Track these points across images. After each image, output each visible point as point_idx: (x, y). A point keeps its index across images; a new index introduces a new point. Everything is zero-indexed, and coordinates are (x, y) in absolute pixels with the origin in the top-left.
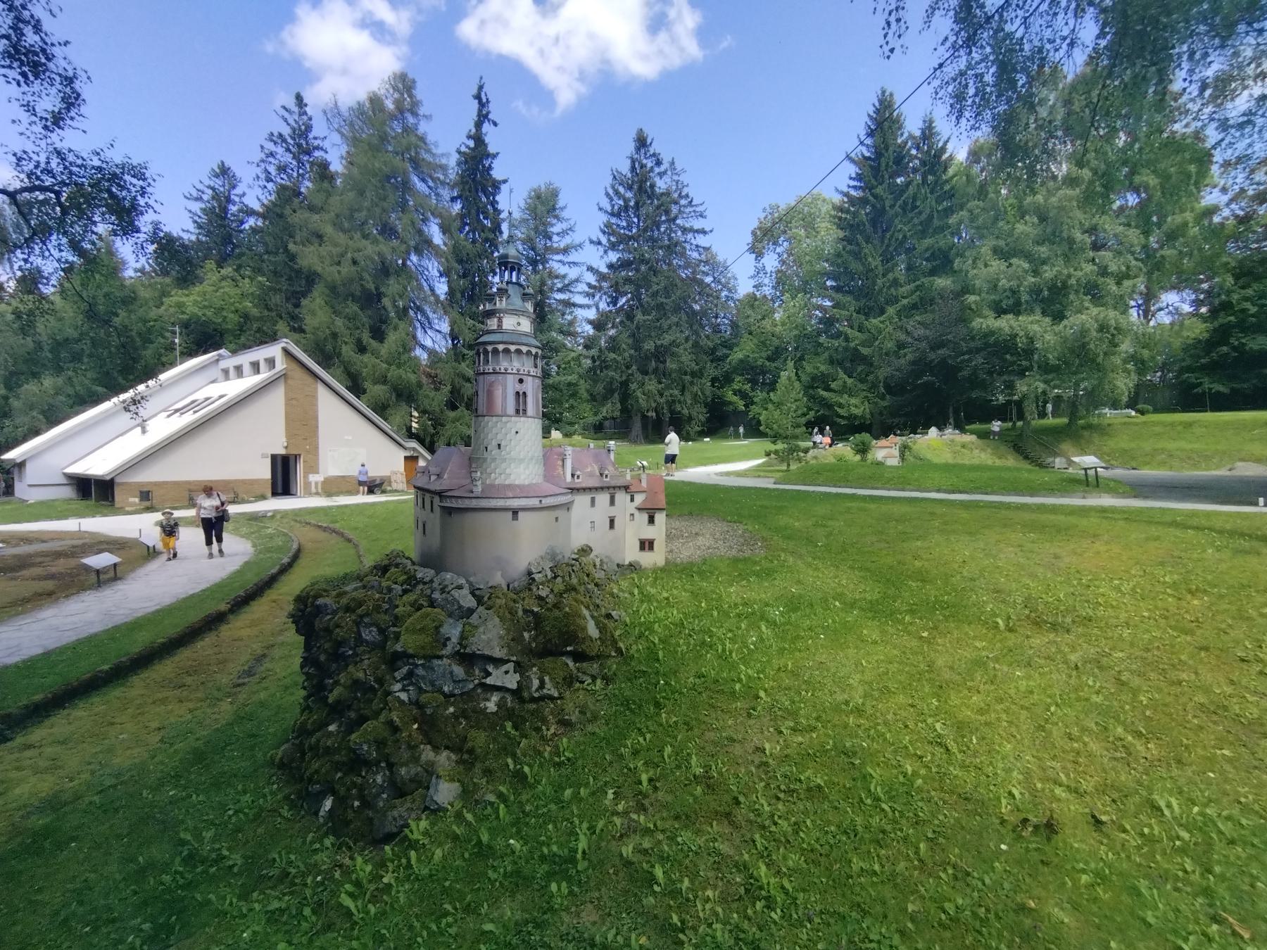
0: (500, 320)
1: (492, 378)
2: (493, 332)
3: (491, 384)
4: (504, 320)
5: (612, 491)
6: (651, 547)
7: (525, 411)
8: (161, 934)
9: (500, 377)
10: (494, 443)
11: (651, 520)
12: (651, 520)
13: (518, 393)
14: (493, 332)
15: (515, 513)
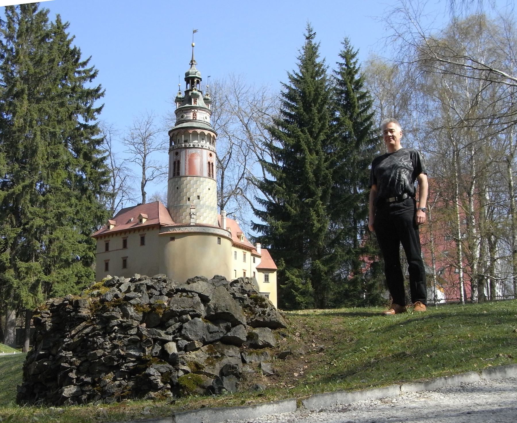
0: (195, 115)
1: (193, 151)
2: (190, 121)
3: (192, 155)
4: (198, 114)
9: (199, 151)
10: (195, 195)
11: (267, 279)
12: (267, 279)
13: (209, 163)
14: (190, 121)
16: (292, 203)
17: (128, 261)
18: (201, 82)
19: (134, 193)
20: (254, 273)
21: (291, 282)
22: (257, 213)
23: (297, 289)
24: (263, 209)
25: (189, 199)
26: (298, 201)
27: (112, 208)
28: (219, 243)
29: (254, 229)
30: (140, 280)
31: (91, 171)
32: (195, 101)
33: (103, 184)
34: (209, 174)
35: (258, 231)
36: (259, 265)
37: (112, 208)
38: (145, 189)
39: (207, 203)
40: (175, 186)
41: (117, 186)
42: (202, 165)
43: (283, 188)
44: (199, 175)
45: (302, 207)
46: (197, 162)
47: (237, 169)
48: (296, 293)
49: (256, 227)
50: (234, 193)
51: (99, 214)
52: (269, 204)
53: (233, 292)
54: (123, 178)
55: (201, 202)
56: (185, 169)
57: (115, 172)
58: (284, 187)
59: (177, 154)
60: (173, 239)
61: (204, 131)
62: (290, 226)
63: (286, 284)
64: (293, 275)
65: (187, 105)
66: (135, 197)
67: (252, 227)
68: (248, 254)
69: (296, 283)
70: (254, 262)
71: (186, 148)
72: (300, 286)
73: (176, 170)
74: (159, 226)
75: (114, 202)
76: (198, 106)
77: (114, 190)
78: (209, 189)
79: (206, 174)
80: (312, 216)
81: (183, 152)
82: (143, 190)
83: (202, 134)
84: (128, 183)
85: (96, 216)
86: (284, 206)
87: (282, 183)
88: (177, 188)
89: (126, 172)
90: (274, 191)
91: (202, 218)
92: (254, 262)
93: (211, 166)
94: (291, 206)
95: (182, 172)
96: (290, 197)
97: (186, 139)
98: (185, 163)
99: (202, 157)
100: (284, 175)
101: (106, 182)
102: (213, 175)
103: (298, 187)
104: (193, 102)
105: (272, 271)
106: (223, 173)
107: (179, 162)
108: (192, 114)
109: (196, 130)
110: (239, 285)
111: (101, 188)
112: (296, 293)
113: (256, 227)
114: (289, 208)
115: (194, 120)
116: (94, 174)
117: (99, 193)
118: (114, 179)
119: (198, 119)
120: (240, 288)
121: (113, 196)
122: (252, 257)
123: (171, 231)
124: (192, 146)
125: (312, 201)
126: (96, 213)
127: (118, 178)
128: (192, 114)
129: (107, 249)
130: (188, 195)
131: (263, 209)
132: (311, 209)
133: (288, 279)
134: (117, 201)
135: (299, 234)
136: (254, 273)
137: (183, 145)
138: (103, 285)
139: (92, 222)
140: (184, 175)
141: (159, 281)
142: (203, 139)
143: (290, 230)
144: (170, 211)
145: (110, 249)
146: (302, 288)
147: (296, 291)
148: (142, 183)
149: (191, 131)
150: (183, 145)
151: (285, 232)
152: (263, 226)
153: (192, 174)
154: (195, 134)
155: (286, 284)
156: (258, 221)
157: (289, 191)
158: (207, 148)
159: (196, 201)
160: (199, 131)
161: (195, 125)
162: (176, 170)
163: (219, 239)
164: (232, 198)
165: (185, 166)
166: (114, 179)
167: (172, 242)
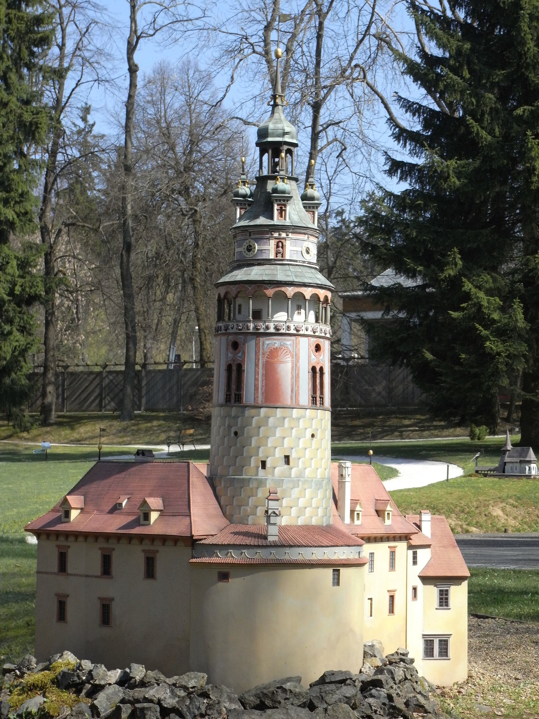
0: (280, 245)
1: (276, 342)
2: (268, 262)
3: (273, 353)
4: (288, 243)
5: (62, 541)
6: (444, 652)
7: (322, 403)
8: (536, 593)
9: (289, 342)
10: (279, 454)
11: (444, 601)
12: (444, 601)
13: (314, 369)
14: (268, 262)
15: (337, 567)
16: (483, 115)
17: (116, 610)
18: (295, 150)
19: (109, 65)
20: (415, 589)
21: (475, 305)
22: (402, 135)
23: (488, 323)
24: (413, 124)
25: (264, 464)
26: (497, 111)
27: (58, 101)
28: (337, 581)
29: (391, 172)
30: (143, 684)
31: (7, 15)
32: (282, 211)
33: (36, 46)
34: (314, 399)
35: (401, 179)
36: (427, 566)
37: (58, 101)
38: (137, 57)
39: (307, 472)
40: (230, 427)
41: (70, 47)
42: (296, 377)
43: (462, 77)
44: (288, 402)
45: (505, 125)
46: (285, 369)
47: (354, 13)
48: (485, 332)
49: (396, 167)
50: (343, 75)
51: (27, 117)
52: (430, 118)
53: (369, 712)
54: (83, 27)
55: (294, 472)
56: (256, 389)
57: (66, 11)
58: (466, 74)
59: (235, 346)
60: (224, 576)
61: (303, 290)
62: (477, 171)
63: (463, 309)
64: (479, 288)
65: (262, 221)
66: (113, 77)
67: (387, 168)
68: (401, 547)
69: (488, 308)
70: (415, 563)
71: (257, 334)
72: (496, 316)
73: (233, 387)
74: (191, 542)
75: (61, 89)
76: (288, 222)
77: (62, 57)
78: (313, 436)
79: (305, 397)
80: (530, 150)
81: (251, 344)
82: (130, 58)
83: (300, 296)
84: (97, 40)
85: (22, 124)
86: (462, 119)
87: (461, 66)
88: (236, 433)
89: (91, 13)
90: (441, 86)
91: (294, 511)
92: (415, 563)
93: (318, 375)
94: (479, 121)
95: (249, 394)
96: (478, 102)
97: (258, 307)
98: (256, 373)
99: (296, 358)
100: (467, 46)
101: (45, 41)
102: (322, 398)
103: (499, 75)
104: (276, 213)
105: (457, 580)
106: (321, 24)
107: (240, 367)
108: (273, 243)
109: (283, 289)
110: (383, 692)
111: (32, 54)
112: (485, 332)
113: (396, 167)
114: (476, 127)
115: (280, 260)
116: (15, 21)
117: (30, 66)
118: (63, 30)
119: (287, 257)
120: (387, 701)
121: (59, 74)
122: (411, 552)
123: (220, 558)
124: (272, 330)
125: (532, 112)
126: (20, 116)
127: (70, 28)
128: (273, 243)
129: (63, 567)
130: (261, 455)
131: (413, 124)
132: (529, 133)
133: (467, 297)
134: (69, 84)
135: (497, 189)
136: (415, 589)
137: (251, 326)
138: (53, 682)
139: (12, 138)
140: (251, 402)
141: (190, 693)
142: (299, 308)
143: (476, 179)
144: (218, 488)
145: (70, 570)
146: (500, 321)
147: (486, 327)
148: (129, 43)
149: (270, 292)
150: (251, 326)
151: (465, 185)
152: (412, 167)
153: (271, 398)
154: (281, 300)
155: (463, 309)
156: (403, 154)
157: (476, 83)
158: (310, 332)
159: (281, 469)
160: (290, 291)
161: (280, 274)
162: (233, 387)
163: (337, 572)
164: (342, 90)
165: (256, 380)
166: (63, 30)
167: (221, 585)
